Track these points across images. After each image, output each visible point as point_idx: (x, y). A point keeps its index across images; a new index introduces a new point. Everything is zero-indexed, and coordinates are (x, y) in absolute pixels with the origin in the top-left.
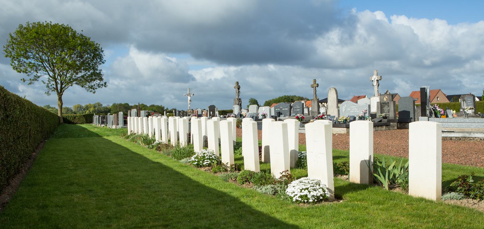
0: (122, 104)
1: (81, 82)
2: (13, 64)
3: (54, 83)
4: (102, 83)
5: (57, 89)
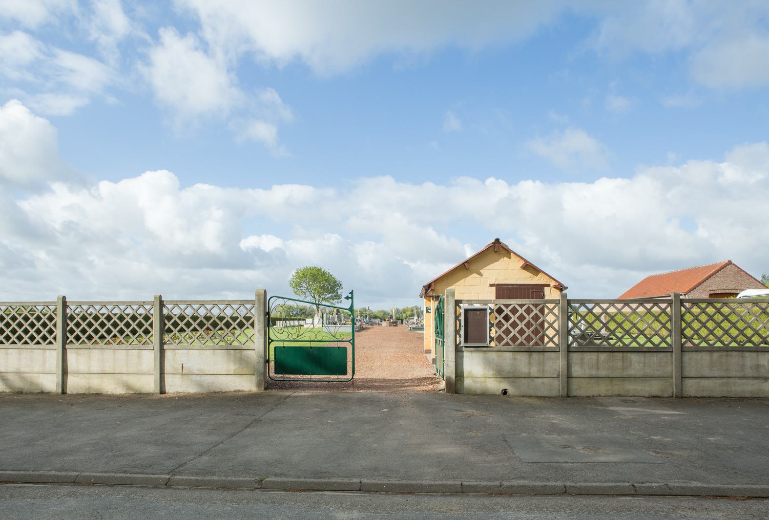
4: (339, 301)
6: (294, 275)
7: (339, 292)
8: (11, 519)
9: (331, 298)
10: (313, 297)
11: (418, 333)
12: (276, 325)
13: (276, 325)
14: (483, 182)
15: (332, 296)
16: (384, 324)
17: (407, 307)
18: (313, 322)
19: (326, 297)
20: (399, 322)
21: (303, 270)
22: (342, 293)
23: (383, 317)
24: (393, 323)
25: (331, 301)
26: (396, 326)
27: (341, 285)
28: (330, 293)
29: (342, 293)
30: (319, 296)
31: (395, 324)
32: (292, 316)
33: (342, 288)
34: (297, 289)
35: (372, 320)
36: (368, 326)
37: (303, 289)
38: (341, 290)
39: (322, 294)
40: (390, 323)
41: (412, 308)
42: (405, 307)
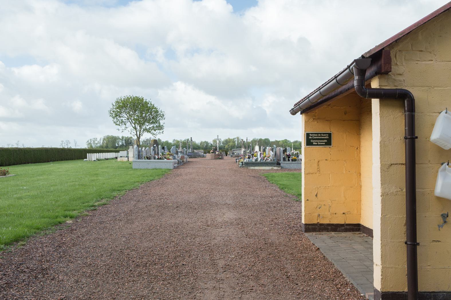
0: (262, 139)
1: (148, 131)
2: (114, 120)
3: (135, 131)
4: (161, 131)
5: (137, 135)
6: (114, 104)
7: (162, 122)
8: (329, 299)
9: (153, 128)
10: (134, 128)
11: (252, 170)
12: (86, 158)
13: (86, 158)
14: (357, 76)
15: (153, 127)
16: (208, 156)
17: (229, 138)
18: (128, 154)
19: (148, 127)
20: (224, 153)
21: (124, 99)
22: (164, 123)
23: (207, 148)
24: (218, 155)
25: (153, 131)
26: (222, 159)
27: (163, 115)
28: (153, 123)
29: (164, 123)
30: (140, 127)
31: (219, 157)
32: (117, 147)
33: (164, 119)
34: (117, 119)
35: (196, 151)
36: (189, 160)
37: (123, 119)
38: (164, 120)
39: (143, 124)
40: (215, 155)
41: (234, 139)
42: (227, 138)
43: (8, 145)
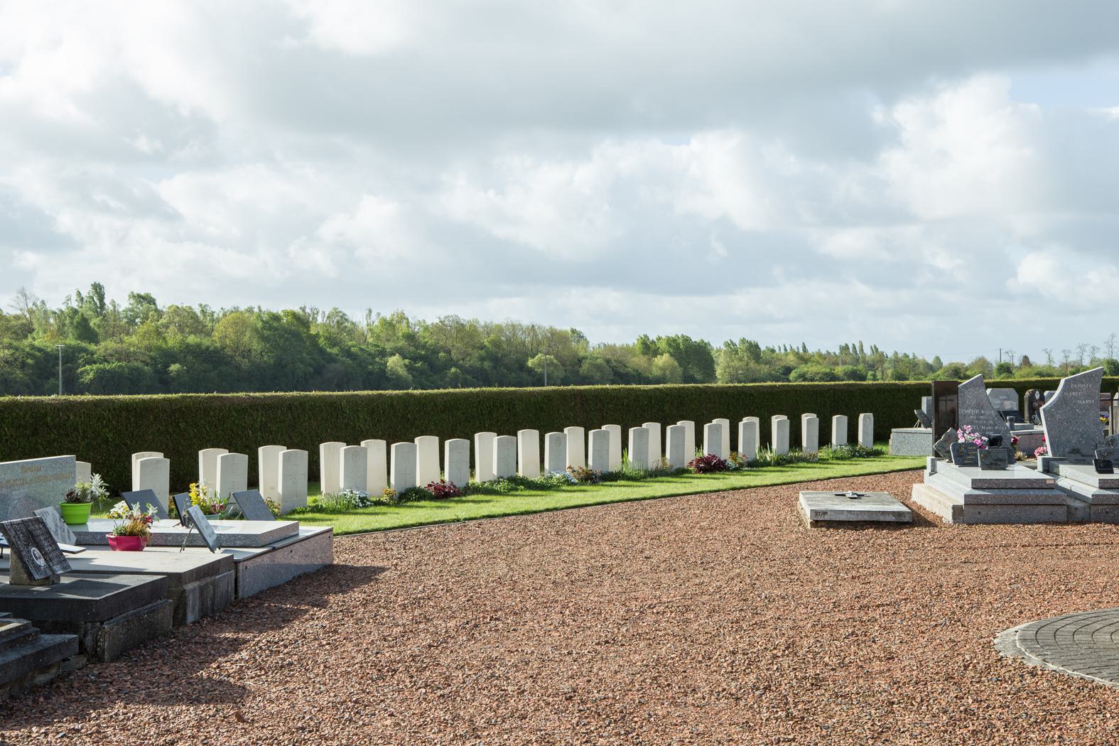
43: (1080, 347)
